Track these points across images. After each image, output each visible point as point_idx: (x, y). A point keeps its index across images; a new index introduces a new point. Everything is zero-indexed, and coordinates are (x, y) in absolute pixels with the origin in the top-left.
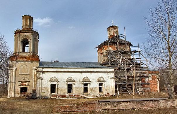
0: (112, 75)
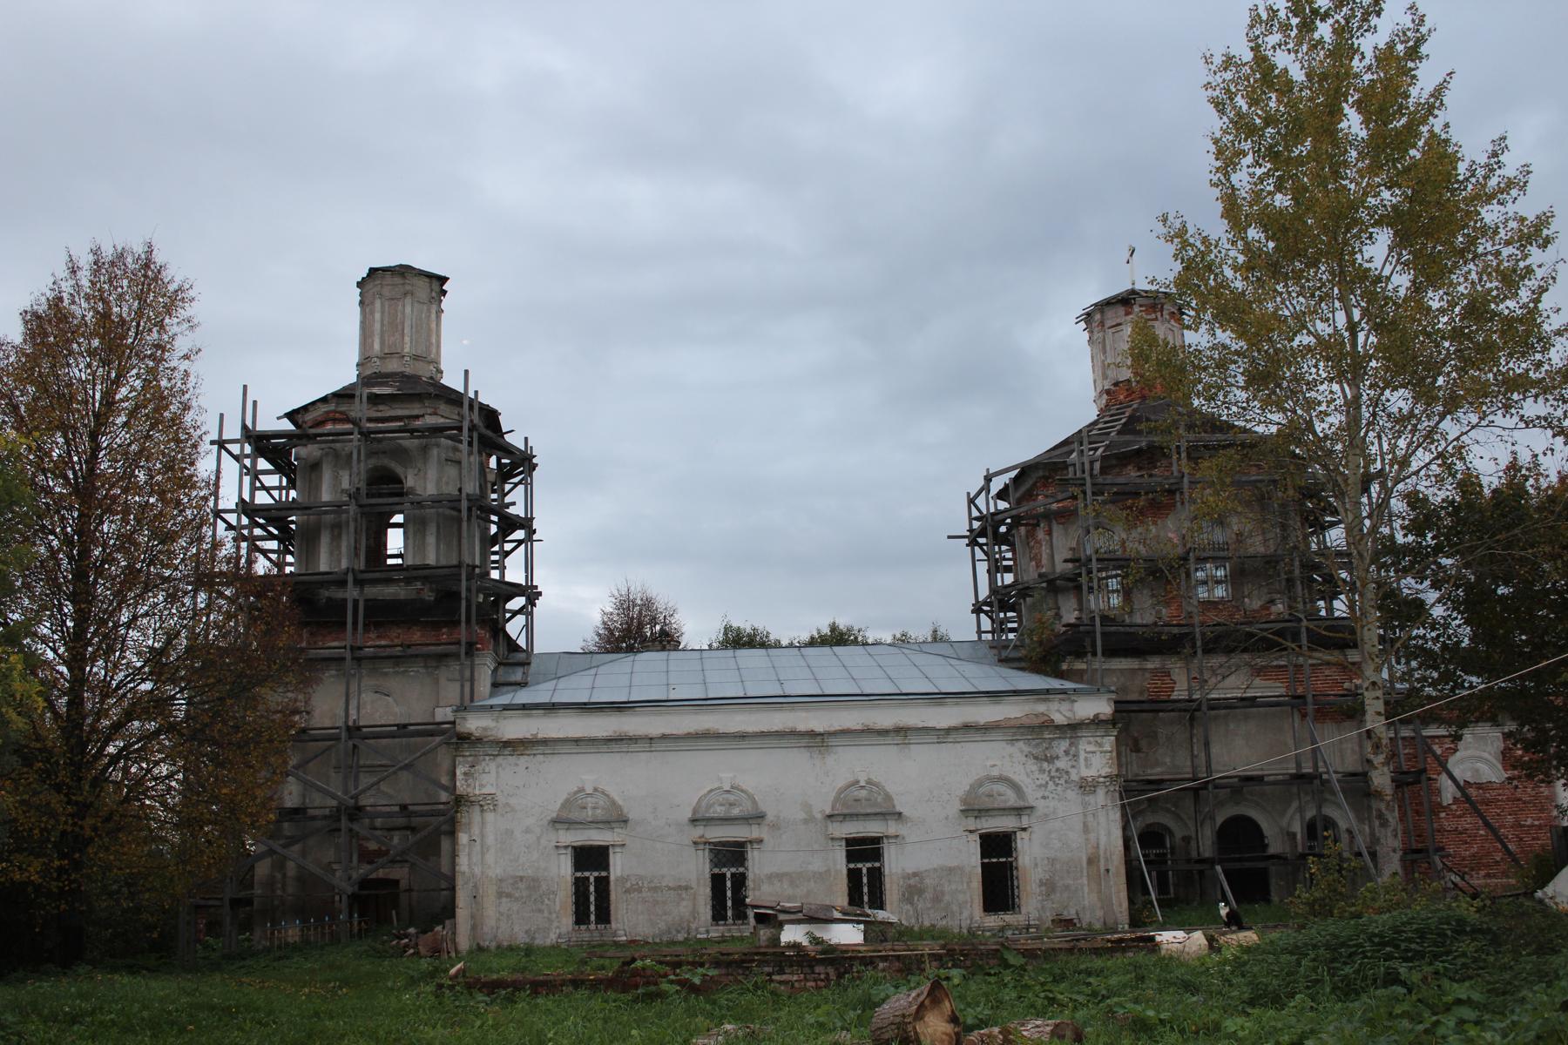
0: (1096, 758)
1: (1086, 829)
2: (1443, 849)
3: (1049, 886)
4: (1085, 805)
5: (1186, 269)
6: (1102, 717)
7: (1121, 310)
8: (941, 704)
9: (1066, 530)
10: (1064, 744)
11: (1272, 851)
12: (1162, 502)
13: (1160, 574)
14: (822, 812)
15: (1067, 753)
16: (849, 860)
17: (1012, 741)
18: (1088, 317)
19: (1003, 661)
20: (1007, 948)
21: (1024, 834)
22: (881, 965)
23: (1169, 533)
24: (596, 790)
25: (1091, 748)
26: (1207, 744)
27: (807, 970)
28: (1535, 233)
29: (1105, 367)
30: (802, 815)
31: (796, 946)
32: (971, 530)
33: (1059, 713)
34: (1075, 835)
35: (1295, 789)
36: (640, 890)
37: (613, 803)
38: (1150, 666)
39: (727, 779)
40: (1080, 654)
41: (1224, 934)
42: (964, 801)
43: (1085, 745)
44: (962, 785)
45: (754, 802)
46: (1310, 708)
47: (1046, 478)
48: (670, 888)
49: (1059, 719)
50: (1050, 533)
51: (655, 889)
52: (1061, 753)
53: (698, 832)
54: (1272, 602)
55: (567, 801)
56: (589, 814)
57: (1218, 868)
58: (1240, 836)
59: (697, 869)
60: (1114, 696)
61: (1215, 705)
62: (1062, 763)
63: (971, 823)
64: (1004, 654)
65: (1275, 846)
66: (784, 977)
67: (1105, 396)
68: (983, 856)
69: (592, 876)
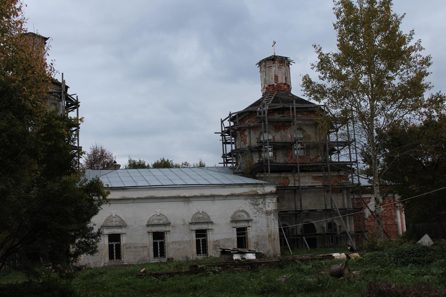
0: (271, 205)
1: (268, 226)
2: (367, 231)
3: (257, 244)
4: (268, 219)
6: (273, 192)
7: (272, 62)
8: (225, 188)
10: (261, 200)
11: (317, 232)
13: (286, 147)
15: (262, 203)
16: (196, 237)
17: (246, 199)
18: (260, 64)
19: (235, 173)
21: (250, 228)
23: (289, 135)
24: (116, 216)
25: (269, 201)
26: (301, 200)
28: (426, 62)
29: (265, 81)
30: (182, 223)
31: (237, 260)
32: (222, 131)
33: (260, 191)
34: (264, 227)
36: (131, 248)
37: (122, 220)
38: (282, 176)
39: (158, 211)
40: (262, 172)
41: (350, 254)
42: (232, 218)
43: (268, 201)
45: (167, 219)
46: (330, 189)
47: (249, 115)
48: (140, 247)
49: (260, 192)
50: (250, 133)
53: (150, 229)
54: (318, 156)
55: (107, 219)
56: (114, 224)
57: (304, 238)
58: (309, 228)
59: (149, 240)
62: (260, 206)
63: (234, 225)
64: (235, 171)
66: (237, 269)
68: (154, 239)
69: (114, 244)
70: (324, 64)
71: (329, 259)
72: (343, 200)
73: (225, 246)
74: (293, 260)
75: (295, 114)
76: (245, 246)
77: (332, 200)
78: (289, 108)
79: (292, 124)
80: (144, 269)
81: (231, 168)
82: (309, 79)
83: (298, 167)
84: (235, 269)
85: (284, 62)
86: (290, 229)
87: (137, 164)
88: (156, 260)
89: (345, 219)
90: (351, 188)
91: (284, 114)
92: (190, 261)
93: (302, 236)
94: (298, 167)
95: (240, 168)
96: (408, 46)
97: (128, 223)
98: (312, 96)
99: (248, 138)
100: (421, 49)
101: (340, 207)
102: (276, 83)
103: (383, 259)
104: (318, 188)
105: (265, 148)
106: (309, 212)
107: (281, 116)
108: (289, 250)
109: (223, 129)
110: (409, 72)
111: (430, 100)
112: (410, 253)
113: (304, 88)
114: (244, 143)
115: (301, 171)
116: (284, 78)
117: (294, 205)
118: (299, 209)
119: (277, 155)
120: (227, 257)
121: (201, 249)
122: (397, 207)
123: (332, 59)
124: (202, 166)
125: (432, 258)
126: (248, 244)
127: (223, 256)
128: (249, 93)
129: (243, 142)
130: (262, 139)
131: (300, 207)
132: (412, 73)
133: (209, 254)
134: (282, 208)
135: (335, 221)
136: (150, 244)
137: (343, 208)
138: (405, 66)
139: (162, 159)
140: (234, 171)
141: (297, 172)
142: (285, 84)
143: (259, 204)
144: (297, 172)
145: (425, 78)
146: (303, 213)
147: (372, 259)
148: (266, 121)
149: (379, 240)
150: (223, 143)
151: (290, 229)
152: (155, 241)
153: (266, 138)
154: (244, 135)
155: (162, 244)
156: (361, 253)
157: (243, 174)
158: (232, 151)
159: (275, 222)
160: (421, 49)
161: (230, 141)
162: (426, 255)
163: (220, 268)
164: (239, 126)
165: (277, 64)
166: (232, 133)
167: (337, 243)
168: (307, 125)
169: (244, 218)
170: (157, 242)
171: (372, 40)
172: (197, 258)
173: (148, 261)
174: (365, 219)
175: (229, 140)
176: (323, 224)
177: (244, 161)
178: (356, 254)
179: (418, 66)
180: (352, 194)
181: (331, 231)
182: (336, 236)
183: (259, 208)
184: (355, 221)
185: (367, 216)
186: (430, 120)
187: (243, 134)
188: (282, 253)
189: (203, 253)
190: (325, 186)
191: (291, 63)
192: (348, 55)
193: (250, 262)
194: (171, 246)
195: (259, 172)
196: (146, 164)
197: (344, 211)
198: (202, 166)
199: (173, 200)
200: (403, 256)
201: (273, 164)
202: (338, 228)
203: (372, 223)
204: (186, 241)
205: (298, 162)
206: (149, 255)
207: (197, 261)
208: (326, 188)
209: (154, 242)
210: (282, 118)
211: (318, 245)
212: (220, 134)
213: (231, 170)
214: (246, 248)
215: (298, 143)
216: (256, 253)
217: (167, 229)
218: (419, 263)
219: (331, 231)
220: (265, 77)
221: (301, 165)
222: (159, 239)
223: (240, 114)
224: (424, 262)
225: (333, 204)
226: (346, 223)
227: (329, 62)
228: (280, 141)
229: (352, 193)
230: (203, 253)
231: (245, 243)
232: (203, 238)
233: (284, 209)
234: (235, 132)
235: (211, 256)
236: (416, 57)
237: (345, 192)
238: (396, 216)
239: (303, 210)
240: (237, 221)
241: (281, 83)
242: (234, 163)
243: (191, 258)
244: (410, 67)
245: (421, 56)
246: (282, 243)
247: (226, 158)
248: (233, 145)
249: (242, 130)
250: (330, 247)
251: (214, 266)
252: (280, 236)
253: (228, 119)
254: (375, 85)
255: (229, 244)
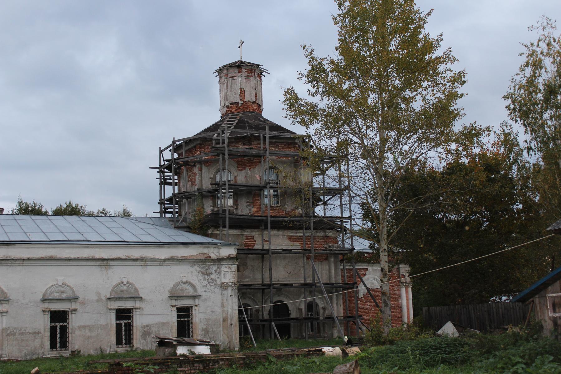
0: (228, 274)
1: (223, 306)
2: (361, 316)
4: (223, 295)
5: (313, 69)
6: (232, 256)
7: (237, 70)
8: (162, 248)
9: (209, 169)
10: (215, 268)
11: (292, 316)
12: (253, 160)
13: (253, 192)
14: (105, 296)
16: (117, 319)
18: (220, 71)
20: (269, 355)
21: (196, 307)
22: (221, 363)
25: (226, 270)
27: (191, 365)
28: (459, 79)
29: (226, 97)
30: (96, 298)
31: (183, 355)
32: (161, 166)
33: (213, 253)
34: (218, 308)
35: (303, 290)
36: (14, 334)
38: (246, 233)
39: (60, 280)
40: (217, 227)
41: (347, 348)
42: (170, 292)
43: (224, 268)
44: (170, 285)
45: (73, 291)
46: (313, 255)
47: (201, 144)
48: (30, 333)
49: (213, 256)
50: (201, 170)
51: (22, 334)
52: (213, 272)
53: (46, 305)
54: (297, 208)
57: (273, 323)
58: (281, 310)
60: (237, 247)
61: (275, 252)
62: (213, 276)
63: (174, 303)
64: (178, 224)
65: (294, 314)
66: (182, 369)
67: (226, 109)
68: (51, 322)
70: (316, 74)
71: (318, 355)
72: (330, 272)
73: (159, 334)
74: (266, 357)
75: (267, 146)
76: (189, 334)
77: (314, 270)
78: (260, 136)
79: (262, 159)
80: (36, 369)
81: (171, 220)
82: (294, 93)
83: (269, 221)
84: (179, 369)
85: (254, 71)
86: (254, 310)
87: (30, 209)
88: (54, 354)
89: (331, 298)
90: (341, 254)
91: (251, 145)
92: (107, 356)
93: (270, 321)
94: (269, 221)
95: (184, 220)
96: (434, 57)
97: (13, 297)
98: (298, 119)
99: (197, 177)
100: (454, 60)
101: (325, 282)
102: (241, 100)
103: (398, 356)
104: (296, 253)
105: (223, 193)
106: (282, 287)
107: (247, 147)
108: (252, 340)
109: (162, 163)
110: (435, 92)
111: (462, 133)
112: (437, 349)
113: (286, 107)
114: (192, 185)
115: (273, 228)
116: (253, 95)
117: (260, 277)
118: (267, 282)
119: (239, 203)
120: (168, 350)
121: (124, 337)
122: (402, 283)
123: (327, 66)
124: (126, 215)
125: (467, 356)
126: (192, 332)
127: (162, 349)
128: (202, 114)
129: (190, 183)
130: (218, 180)
131: (269, 280)
132: (439, 93)
133: (135, 345)
134: (243, 280)
135: (318, 301)
136: (45, 329)
137: (328, 282)
138: (429, 83)
139: (68, 203)
140: (175, 224)
141: (266, 228)
142: (254, 103)
143: (212, 273)
144: (266, 228)
145: (458, 101)
146: (273, 288)
147: (382, 356)
148: (226, 154)
149: (386, 330)
150: (161, 183)
151: (254, 310)
152: (53, 324)
153: (224, 179)
154: (193, 173)
155: (64, 330)
156: (363, 346)
157: (190, 229)
158: (174, 194)
159: (234, 299)
160: (454, 60)
161: (171, 181)
162: (459, 351)
163: (157, 367)
164: (186, 159)
165: (244, 73)
166: (176, 169)
167: (319, 332)
168: (283, 163)
169: (189, 293)
170: (56, 326)
171: (383, 44)
172: (116, 352)
173: (40, 356)
174: (358, 298)
175: (170, 179)
176: (299, 305)
177: (190, 211)
178: (356, 349)
179: (448, 84)
180: (341, 263)
181: (311, 315)
182: (318, 321)
183: (211, 279)
184: (344, 302)
185: (361, 295)
186: (456, 161)
187: (191, 171)
188: (242, 347)
189: (125, 344)
190: (306, 250)
191: (264, 73)
192: (351, 63)
193: (201, 359)
194: (77, 332)
195: (212, 226)
196: (43, 210)
197: (331, 287)
198: (126, 215)
199: (84, 263)
200: (427, 353)
201: (234, 216)
202: (321, 311)
203: (368, 305)
204: (101, 325)
205: (269, 215)
206: (42, 345)
207: (115, 355)
208: (306, 253)
209: (51, 327)
210: (248, 151)
211: (292, 335)
212: (158, 170)
213: (171, 223)
214: (189, 337)
215: (271, 187)
216: (211, 345)
217: (73, 306)
218: (450, 363)
219: (311, 315)
220: (226, 90)
221: (272, 219)
222: (59, 322)
223: (188, 141)
224: (457, 361)
225: (316, 276)
226: (332, 303)
227: (324, 71)
228: (244, 183)
229: (342, 261)
230: (125, 344)
231: (189, 329)
232: (126, 321)
233: (246, 281)
234: (179, 168)
235: (137, 348)
236: (445, 71)
237: (332, 260)
238: (400, 296)
239: (273, 284)
240: (178, 297)
241: (249, 101)
242: (177, 213)
243: (108, 352)
244: (437, 85)
245: (451, 71)
246: (243, 331)
247: (164, 204)
248: (176, 187)
249: (190, 165)
250: (309, 338)
251: (148, 365)
252: (240, 321)
253: (171, 148)
254: (386, 109)
255: (164, 332)
